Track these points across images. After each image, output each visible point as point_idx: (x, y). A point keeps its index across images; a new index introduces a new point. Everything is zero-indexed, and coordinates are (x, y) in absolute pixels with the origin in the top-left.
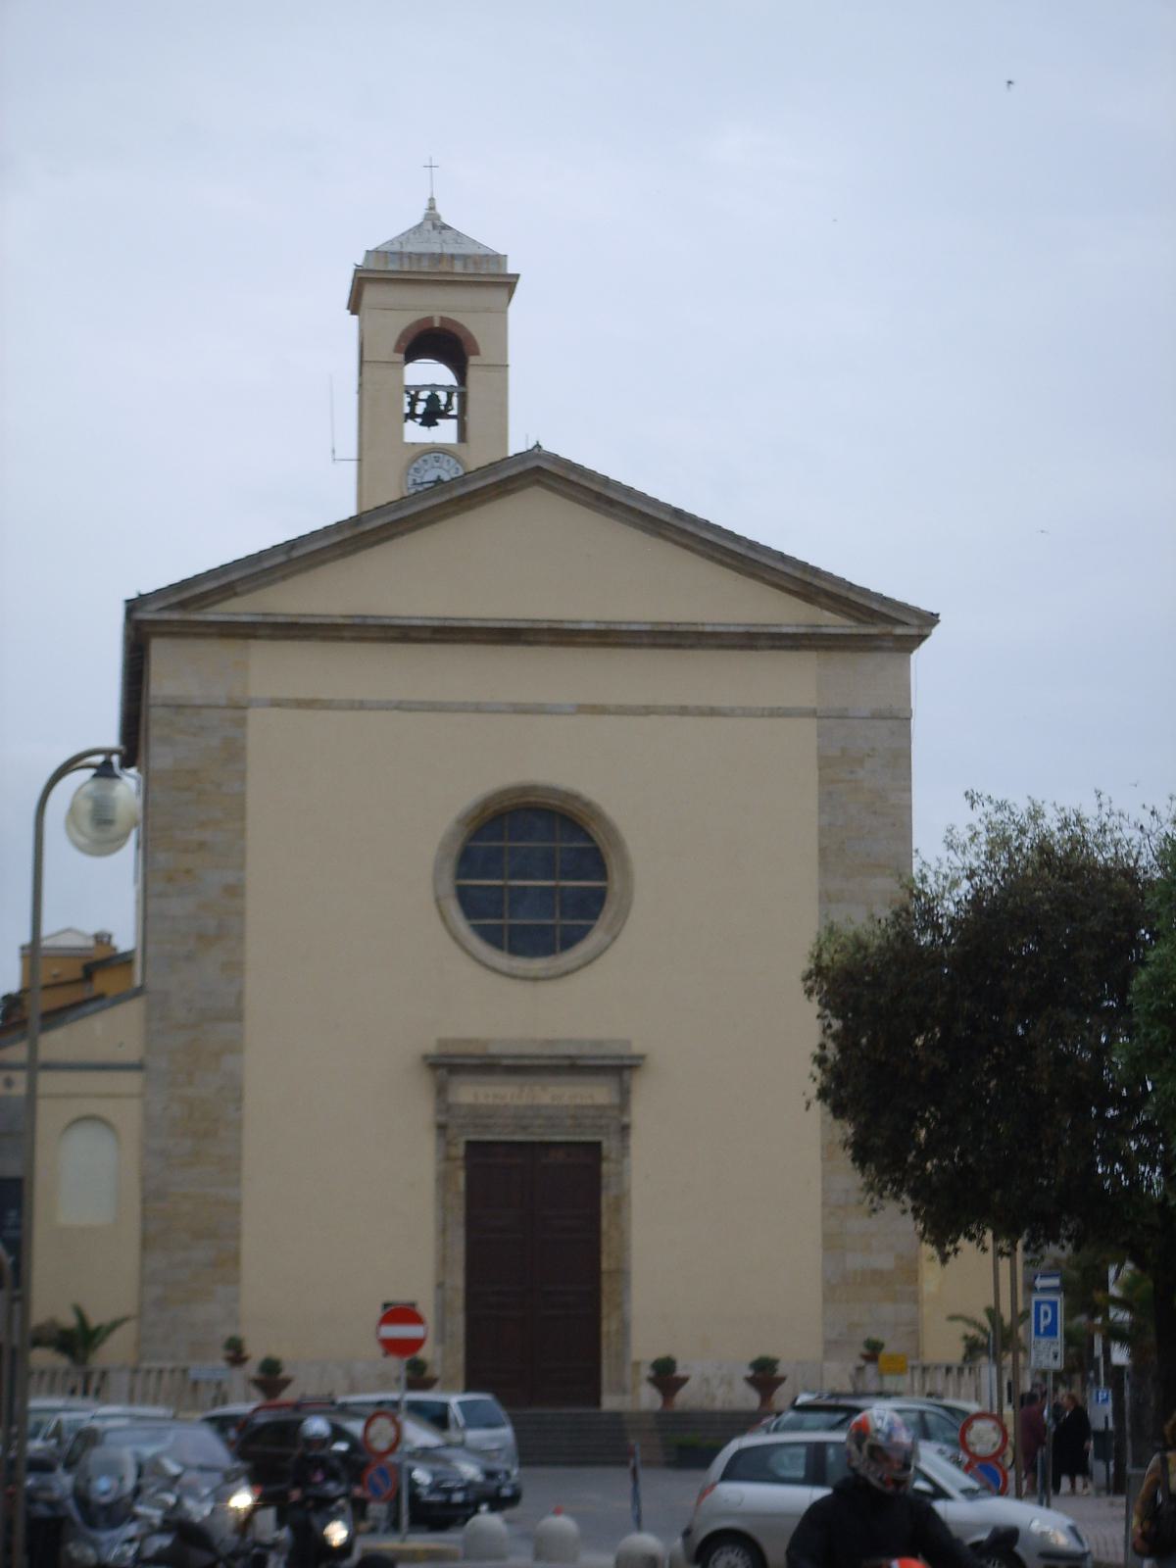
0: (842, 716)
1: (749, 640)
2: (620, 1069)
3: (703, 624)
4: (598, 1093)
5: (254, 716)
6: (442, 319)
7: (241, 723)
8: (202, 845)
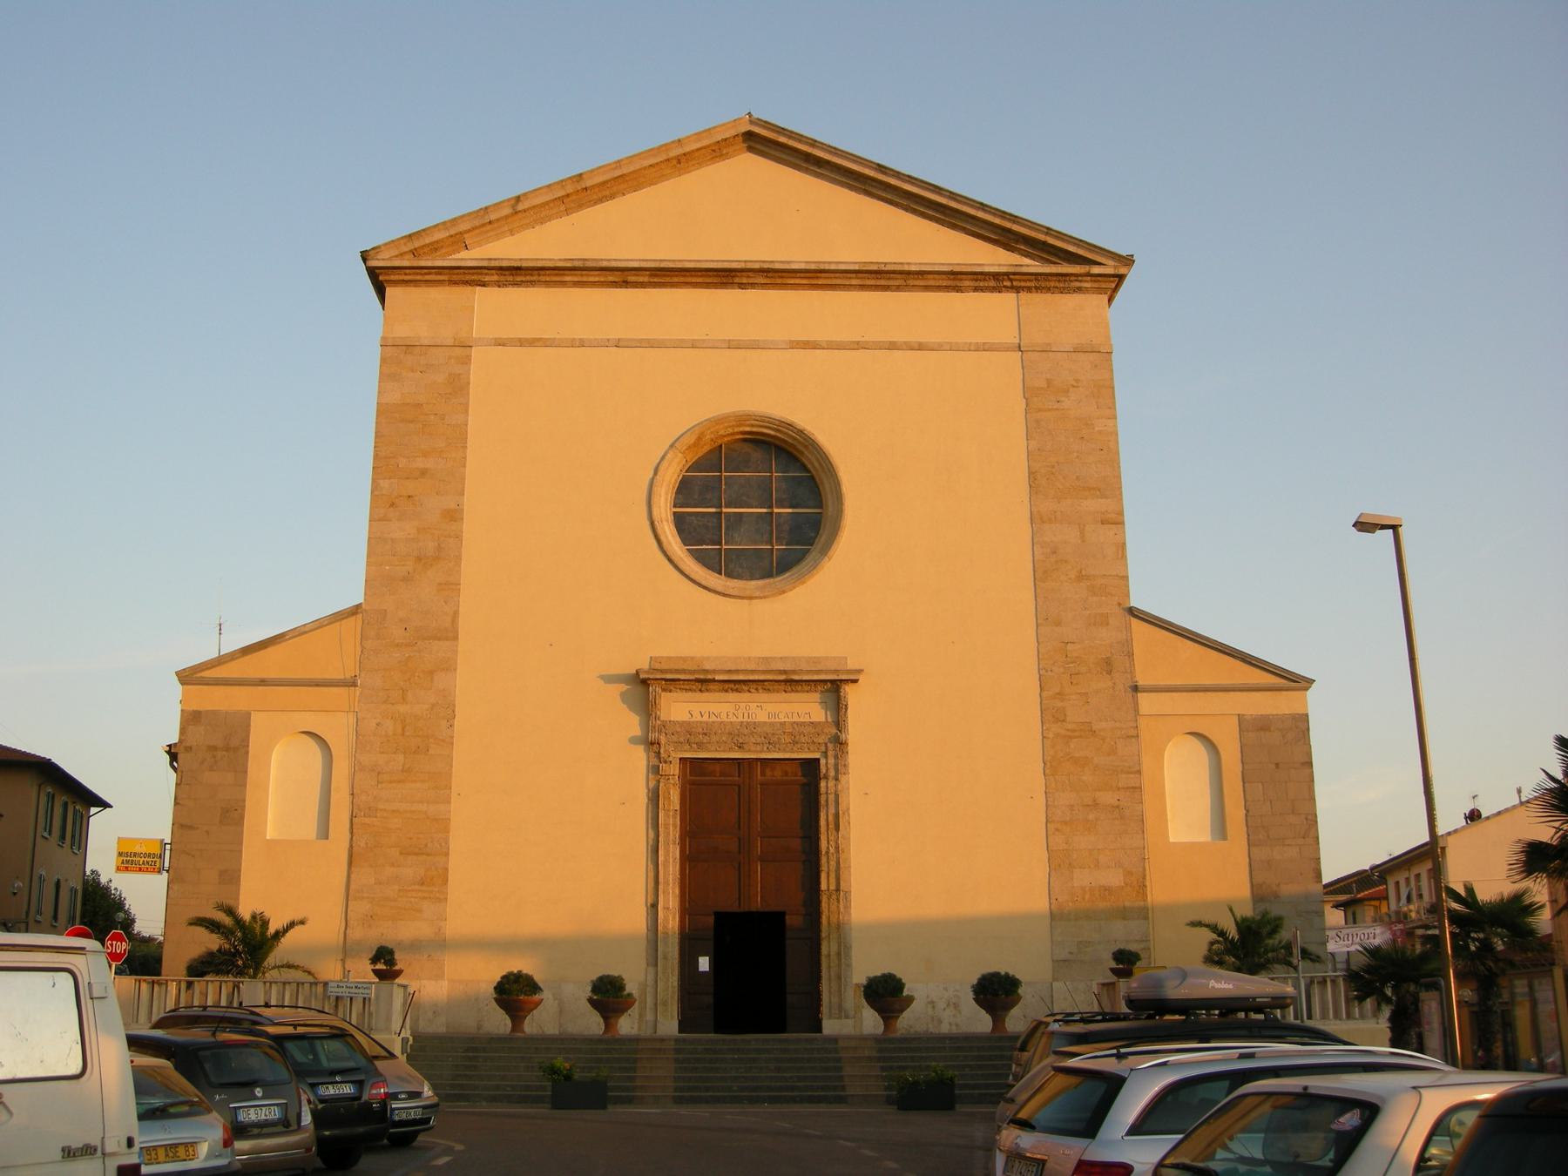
1: (955, 280)
7: (467, 361)
8: (424, 473)
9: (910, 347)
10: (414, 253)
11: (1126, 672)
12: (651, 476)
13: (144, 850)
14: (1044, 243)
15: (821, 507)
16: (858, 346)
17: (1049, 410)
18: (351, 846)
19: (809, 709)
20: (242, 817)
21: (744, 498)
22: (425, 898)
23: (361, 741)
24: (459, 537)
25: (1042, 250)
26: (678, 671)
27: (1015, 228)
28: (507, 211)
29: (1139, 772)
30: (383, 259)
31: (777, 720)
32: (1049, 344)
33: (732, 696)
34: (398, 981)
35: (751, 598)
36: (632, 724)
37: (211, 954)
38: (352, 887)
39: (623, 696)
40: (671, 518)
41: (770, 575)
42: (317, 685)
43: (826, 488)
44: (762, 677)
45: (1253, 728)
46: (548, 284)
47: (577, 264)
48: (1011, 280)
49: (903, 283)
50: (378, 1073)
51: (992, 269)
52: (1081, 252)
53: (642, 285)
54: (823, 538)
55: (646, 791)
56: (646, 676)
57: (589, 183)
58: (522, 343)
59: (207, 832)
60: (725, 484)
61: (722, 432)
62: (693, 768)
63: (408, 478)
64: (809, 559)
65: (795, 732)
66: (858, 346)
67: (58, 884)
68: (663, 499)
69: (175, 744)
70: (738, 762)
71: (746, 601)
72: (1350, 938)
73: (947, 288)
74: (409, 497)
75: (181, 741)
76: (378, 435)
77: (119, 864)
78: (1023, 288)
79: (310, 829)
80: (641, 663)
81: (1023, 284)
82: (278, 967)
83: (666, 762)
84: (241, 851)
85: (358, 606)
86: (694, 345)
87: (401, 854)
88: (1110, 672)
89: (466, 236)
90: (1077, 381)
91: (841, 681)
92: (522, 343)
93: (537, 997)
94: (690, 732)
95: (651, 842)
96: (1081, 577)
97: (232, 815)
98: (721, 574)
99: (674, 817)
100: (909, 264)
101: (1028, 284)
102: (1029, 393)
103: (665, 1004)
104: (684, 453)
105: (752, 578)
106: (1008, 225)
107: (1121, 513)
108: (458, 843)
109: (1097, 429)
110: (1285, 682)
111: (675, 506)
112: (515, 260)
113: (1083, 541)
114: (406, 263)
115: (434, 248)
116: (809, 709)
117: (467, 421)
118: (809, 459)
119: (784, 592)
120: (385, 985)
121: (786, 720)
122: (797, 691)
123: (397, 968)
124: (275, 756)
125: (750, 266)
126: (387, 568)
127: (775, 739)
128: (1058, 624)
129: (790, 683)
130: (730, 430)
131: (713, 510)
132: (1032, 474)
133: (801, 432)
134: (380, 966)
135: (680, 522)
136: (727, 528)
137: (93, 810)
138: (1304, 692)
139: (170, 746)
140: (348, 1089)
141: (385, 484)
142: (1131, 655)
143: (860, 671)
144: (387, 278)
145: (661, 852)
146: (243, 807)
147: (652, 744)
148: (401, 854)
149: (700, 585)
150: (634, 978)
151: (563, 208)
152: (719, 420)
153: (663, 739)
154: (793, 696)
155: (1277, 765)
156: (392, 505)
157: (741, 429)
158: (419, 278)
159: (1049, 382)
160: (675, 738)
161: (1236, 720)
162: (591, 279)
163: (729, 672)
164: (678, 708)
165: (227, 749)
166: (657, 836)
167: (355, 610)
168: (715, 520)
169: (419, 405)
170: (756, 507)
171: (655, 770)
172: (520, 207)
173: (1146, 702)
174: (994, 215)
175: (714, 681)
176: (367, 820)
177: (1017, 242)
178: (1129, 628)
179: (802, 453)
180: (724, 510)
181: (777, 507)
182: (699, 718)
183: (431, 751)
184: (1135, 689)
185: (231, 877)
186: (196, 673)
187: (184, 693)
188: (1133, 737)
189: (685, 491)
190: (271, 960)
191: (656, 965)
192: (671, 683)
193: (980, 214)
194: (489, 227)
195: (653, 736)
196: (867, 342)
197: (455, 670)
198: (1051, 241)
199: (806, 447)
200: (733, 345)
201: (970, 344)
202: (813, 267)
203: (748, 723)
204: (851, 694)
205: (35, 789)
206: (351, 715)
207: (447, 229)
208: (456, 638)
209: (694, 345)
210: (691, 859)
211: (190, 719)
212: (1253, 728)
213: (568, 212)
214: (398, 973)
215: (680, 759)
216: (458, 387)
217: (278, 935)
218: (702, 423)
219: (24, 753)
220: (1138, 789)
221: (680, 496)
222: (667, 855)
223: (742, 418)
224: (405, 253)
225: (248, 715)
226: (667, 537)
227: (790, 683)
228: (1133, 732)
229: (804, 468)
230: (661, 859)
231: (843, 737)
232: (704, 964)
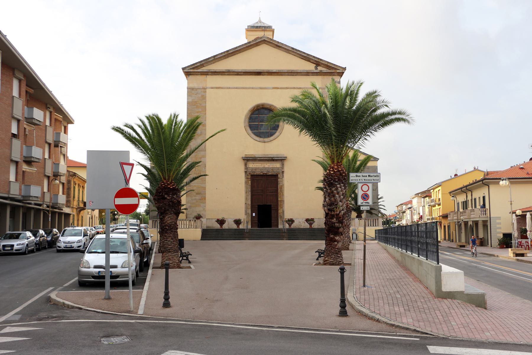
1: (307, 73)
2: (282, 160)
3: (298, 70)
4: (277, 165)
7: (205, 92)
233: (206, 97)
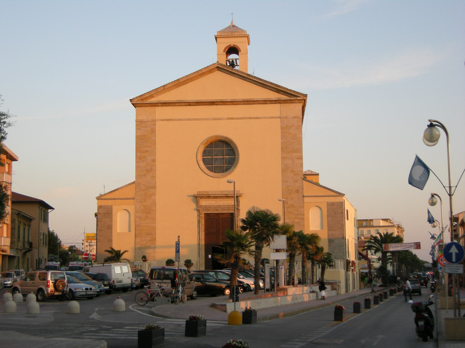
0: (286, 118)
1: (265, 102)
5: (157, 123)
6: (233, 45)
7: (155, 125)
8: (147, 151)
9: (255, 118)
10: (142, 100)
11: (302, 193)
12: (197, 151)
13: (91, 235)
14: (286, 92)
15: (235, 156)
16: (243, 118)
17: (286, 132)
18: (135, 233)
19: (231, 202)
20: (112, 228)
21: (218, 154)
22: (151, 244)
23: (136, 211)
24: (155, 166)
25: (286, 93)
26: (203, 195)
27: (279, 88)
28: (162, 89)
29: (304, 215)
30: (135, 102)
31: (225, 204)
32: (287, 116)
33: (215, 199)
34: (147, 262)
35: (219, 178)
36: (194, 206)
37: (110, 257)
38: (136, 242)
39: (192, 199)
40: (201, 159)
41: (223, 172)
42: (126, 199)
43: (236, 152)
44: (221, 196)
45: (330, 205)
46: (172, 106)
47: (179, 102)
48: (278, 101)
49: (253, 103)
50: (147, 276)
51: (274, 99)
52: (295, 94)
53: (194, 105)
54: (235, 164)
55: (197, 220)
56: (196, 196)
57: (181, 81)
58: (167, 120)
59: (105, 231)
60: (214, 151)
61: (212, 140)
62: (207, 215)
63: (143, 152)
64: (232, 168)
65: (228, 207)
66: (243, 118)
67: (44, 233)
68: (199, 156)
69: (97, 213)
70: (217, 214)
71: (218, 178)
72: (405, 247)
73: (264, 104)
74: (144, 157)
75: (98, 212)
76: (136, 143)
77: (87, 239)
78: (282, 103)
79: (126, 230)
80: (196, 193)
81: (281, 102)
82: (123, 259)
83: (201, 214)
84: (112, 235)
85: (134, 182)
86: (206, 119)
87: (146, 235)
88: (298, 193)
89: (153, 95)
90: (293, 125)
91: (238, 196)
92: (167, 120)
93: (174, 264)
94: (206, 207)
95: (198, 231)
96: (292, 171)
97: (110, 228)
98: (213, 172)
99: (203, 226)
100: (254, 99)
101: (282, 102)
102: (282, 128)
103: (202, 265)
104: (204, 145)
105: (220, 173)
106: (278, 88)
107: (302, 156)
108: (158, 232)
109: (298, 136)
110: (338, 194)
111: (203, 157)
112: (165, 101)
113: (293, 163)
114: (140, 102)
115: (146, 98)
116: (231, 202)
117: (156, 139)
118: (232, 145)
119: (226, 176)
120: (144, 263)
121: (227, 204)
122: (229, 198)
123: (147, 259)
124: (118, 215)
125: (218, 101)
126: (140, 173)
127: (224, 209)
128: (287, 182)
129: (227, 197)
130: (214, 139)
131: (211, 157)
132: (282, 148)
133: (230, 139)
134: (144, 259)
135: (204, 160)
136: (214, 161)
137: (50, 210)
138: (343, 197)
139: (95, 213)
140: (143, 278)
141: (138, 154)
142: (303, 189)
143: (242, 194)
144: (136, 105)
145: (200, 233)
146: (112, 226)
147: (198, 210)
148: (146, 235)
149: (208, 175)
150: (194, 260)
151: (175, 87)
152: (211, 137)
153: (200, 209)
154: (228, 199)
155: (335, 213)
156: (140, 159)
157: (217, 139)
158: (143, 105)
159: (287, 125)
160: (203, 209)
161: (326, 203)
162: (182, 105)
163: (214, 195)
164: (204, 202)
165: (108, 214)
166: (200, 230)
167: (134, 183)
168: (211, 159)
169: (145, 135)
170: (221, 156)
171: (199, 216)
172: (165, 88)
173: (306, 199)
174: (275, 86)
175: (211, 196)
176: (139, 228)
177: (280, 91)
178: (303, 183)
179: (230, 144)
180: (214, 157)
181: (225, 156)
182: (208, 204)
183: (151, 213)
184: (304, 196)
185: (110, 241)
186: (100, 197)
187: (98, 201)
188: (303, 207)
189: (205, 153)
190: (122, 258)
191: (200, 257)
192: (202, 197)
193: (271, 86)
194: (158, 93)
195: (198, 209)
196: (245, 117)
197: (156, 195)
198: (288, 91)
199: (231, 143)
200: (215, 119)
201: (269, 117)
202: (232, 100)
203: (218, 205)
204: (241, 199)
205: (38, 209)
206: (134, 206)
207: (149, 94)
208: (156, 188)
209: (206, 119)
210: (207, 235)
211: (100, 207)
212: (330, 205)
213: (176, 88)
214: (147, 260)
215: (204, 213)
216: (153, 131)
217: (123, 254)
218: (206, 139)
219: (34, 198)
220: (303, 219)
221: (204, 154)
222: (201, 234)
223: (217, 136)
224: (140, 100)
225: (112, 206)
226: (200, 164)
227: (227, 197)
228: (302, 206)
229: (231, 147)
230: (200, 235)
231: (239, 208)
232: (210, 256)
233: (156, 130)
